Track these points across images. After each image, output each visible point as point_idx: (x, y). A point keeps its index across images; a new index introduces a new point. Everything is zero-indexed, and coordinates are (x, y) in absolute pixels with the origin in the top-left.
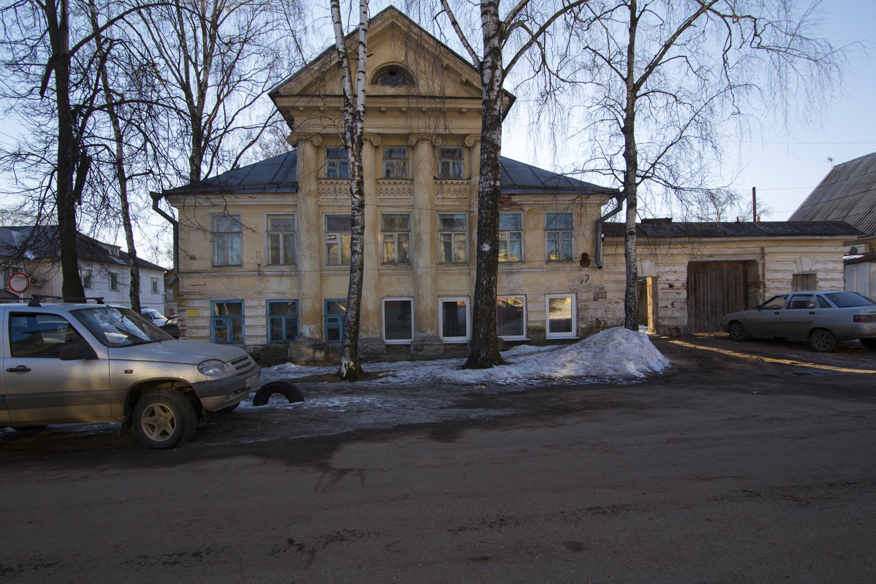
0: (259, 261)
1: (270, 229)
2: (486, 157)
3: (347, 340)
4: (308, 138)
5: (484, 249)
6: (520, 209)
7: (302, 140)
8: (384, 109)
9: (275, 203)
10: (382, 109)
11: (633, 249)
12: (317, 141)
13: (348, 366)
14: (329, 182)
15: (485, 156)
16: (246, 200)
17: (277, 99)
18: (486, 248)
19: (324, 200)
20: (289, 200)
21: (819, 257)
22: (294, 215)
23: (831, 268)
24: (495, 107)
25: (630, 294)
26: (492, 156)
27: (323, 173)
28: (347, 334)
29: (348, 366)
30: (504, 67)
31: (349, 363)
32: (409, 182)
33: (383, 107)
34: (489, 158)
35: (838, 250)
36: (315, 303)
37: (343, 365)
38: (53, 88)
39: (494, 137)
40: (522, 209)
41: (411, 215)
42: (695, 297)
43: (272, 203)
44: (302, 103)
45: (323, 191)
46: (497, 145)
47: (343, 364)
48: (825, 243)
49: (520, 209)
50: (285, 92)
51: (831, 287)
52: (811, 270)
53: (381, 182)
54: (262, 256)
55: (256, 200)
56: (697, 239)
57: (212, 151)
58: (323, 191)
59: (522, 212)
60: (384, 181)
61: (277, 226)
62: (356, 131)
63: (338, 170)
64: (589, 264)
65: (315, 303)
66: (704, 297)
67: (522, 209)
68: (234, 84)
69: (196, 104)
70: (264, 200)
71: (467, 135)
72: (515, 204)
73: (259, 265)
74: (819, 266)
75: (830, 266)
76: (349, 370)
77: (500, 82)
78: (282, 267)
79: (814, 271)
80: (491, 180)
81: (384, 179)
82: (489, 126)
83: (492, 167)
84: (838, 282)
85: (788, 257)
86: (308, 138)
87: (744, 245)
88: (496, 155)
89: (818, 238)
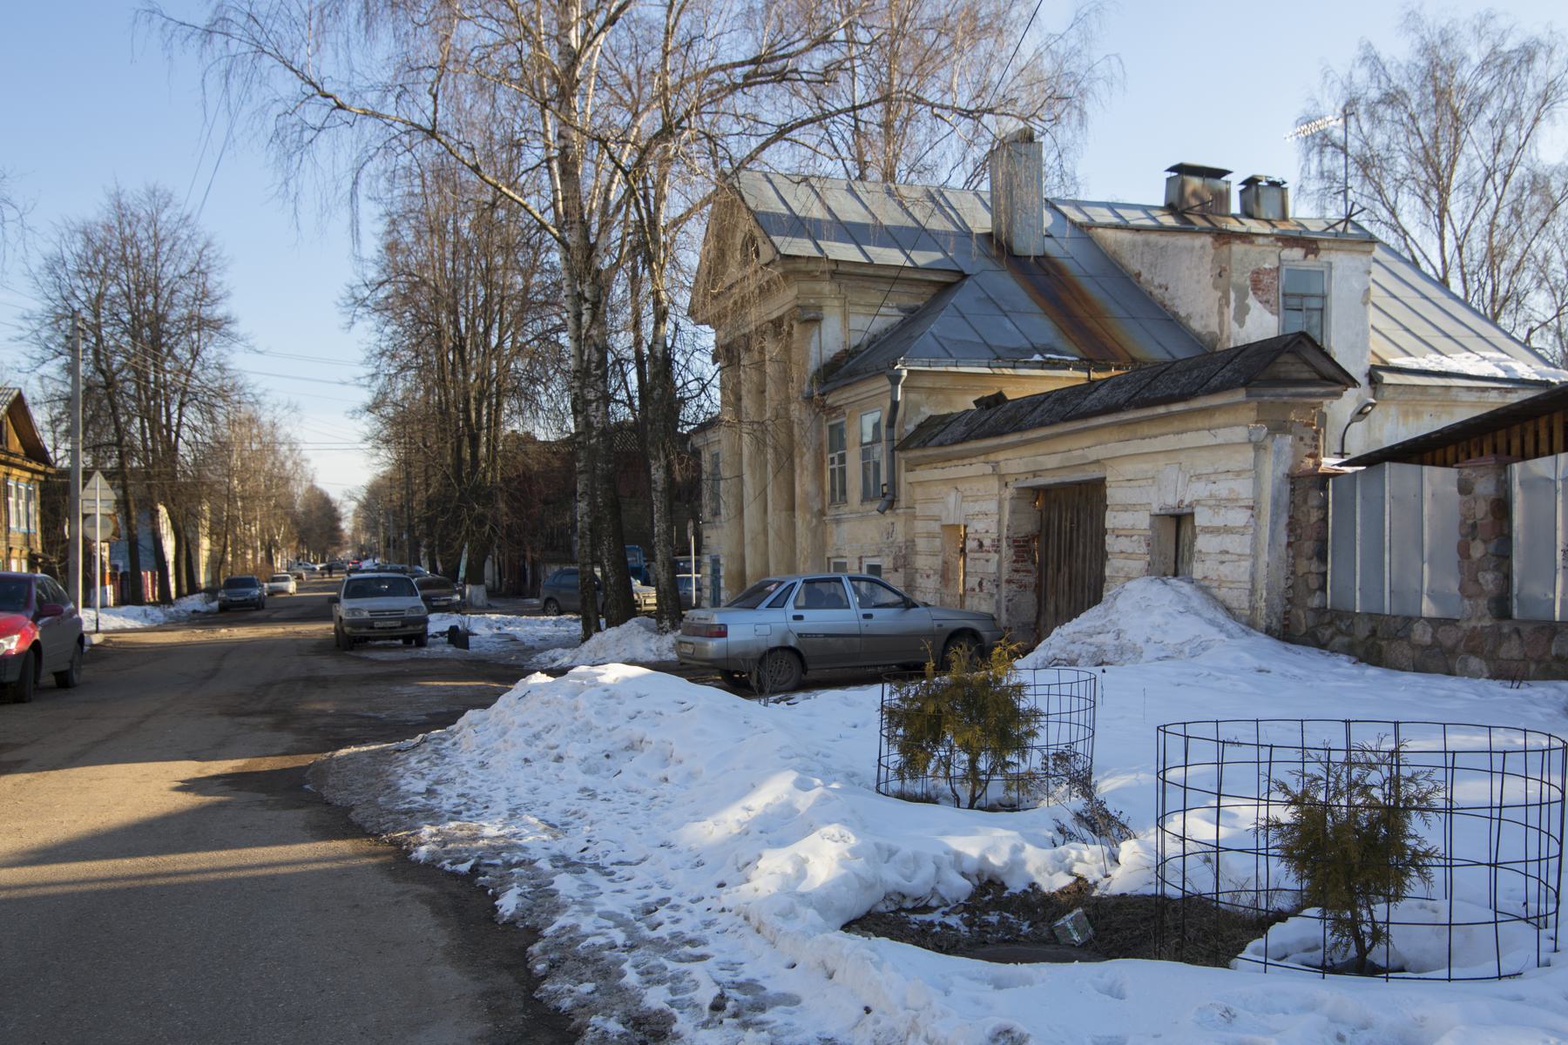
21: (1203, 464)
23: (1224, 493)
35: (1220, 440)
36: (486, 841)
38: (423, 124)
42: (1070, 568)
48: (1220, 419)
51: (1221, 552)
52: (1182, 501)
56: (960, 462)
57: (709, 396)
65: (486, 841)
66: (1084, 569)
68: (620, 217)
74: (1199, 490)
75: (1223, 488)
79: (1190, 505)
84: (1236, 537)
85: (1145, 466)
87: (1062, 446)
89: (1161, 410)
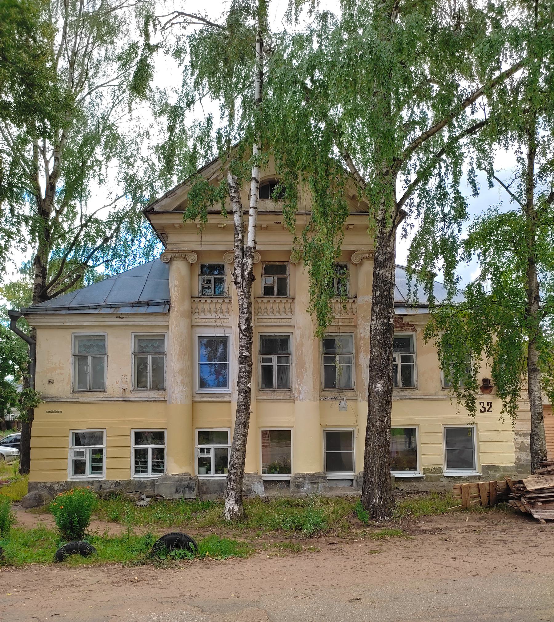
0: (125, 386)
1: (136, 351)
2: (378, 295)
3: (232, 483)
4: (181, 255)
5: (377, 389)
6: (412, 329)
7: (175, 257)
8: (265, 226)
9: (145, 324)
10: (263, 226)
11: (537, 387)
12: (193, 258)
13: (233, 512)
14: (203, 300)
15: (378, 293)
16: (113, 320)
17: (152, 217)
18: (379, 387)
19: (198, 320)
20: (159, 321)
22: (164, 335)
24: (388, 244)
25: (536, 436)
26: (385, 294)
27: (197, 290)
28: (232, 476)
29: (233, 512)
30: (398, 201)
31: (233, 507)
32: (290, 301)
33: (264, 224)
34: (382, 295)
37: (227, 510)
39: (387, 274)
40: (415, 330)
41: (291, 337)
43: (141, 323)
44: (177, 220)
45: (197, 311)
46: (391, 282)
47: (227, 508)
49: (412, 329)
50: (160, 209)
53: (259, 300)
54: (128, 380)
55: (124, 320)
58: (197, 311)
59: (414, 333)
60: (263, 299)
61: (145, 347)
62: (247, 267)
63: (213, 288)
64: (491, 391)
67: (415, 330)
69: (43, 195)
70: (133, 320)
71: (353, 252)
72: (408, 325)
73: (124, 390)
76: (234, 515)
77: (394, 217)
78: (149, 393)
80: (384, 318)
81: (263, 297)
82: (382, 263)
83: (385, 304)
86: (181, 255)
88: (389, 293)
